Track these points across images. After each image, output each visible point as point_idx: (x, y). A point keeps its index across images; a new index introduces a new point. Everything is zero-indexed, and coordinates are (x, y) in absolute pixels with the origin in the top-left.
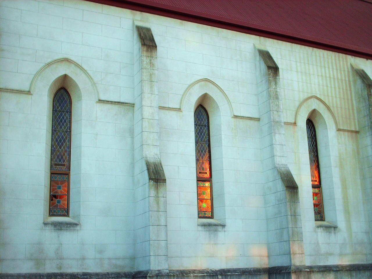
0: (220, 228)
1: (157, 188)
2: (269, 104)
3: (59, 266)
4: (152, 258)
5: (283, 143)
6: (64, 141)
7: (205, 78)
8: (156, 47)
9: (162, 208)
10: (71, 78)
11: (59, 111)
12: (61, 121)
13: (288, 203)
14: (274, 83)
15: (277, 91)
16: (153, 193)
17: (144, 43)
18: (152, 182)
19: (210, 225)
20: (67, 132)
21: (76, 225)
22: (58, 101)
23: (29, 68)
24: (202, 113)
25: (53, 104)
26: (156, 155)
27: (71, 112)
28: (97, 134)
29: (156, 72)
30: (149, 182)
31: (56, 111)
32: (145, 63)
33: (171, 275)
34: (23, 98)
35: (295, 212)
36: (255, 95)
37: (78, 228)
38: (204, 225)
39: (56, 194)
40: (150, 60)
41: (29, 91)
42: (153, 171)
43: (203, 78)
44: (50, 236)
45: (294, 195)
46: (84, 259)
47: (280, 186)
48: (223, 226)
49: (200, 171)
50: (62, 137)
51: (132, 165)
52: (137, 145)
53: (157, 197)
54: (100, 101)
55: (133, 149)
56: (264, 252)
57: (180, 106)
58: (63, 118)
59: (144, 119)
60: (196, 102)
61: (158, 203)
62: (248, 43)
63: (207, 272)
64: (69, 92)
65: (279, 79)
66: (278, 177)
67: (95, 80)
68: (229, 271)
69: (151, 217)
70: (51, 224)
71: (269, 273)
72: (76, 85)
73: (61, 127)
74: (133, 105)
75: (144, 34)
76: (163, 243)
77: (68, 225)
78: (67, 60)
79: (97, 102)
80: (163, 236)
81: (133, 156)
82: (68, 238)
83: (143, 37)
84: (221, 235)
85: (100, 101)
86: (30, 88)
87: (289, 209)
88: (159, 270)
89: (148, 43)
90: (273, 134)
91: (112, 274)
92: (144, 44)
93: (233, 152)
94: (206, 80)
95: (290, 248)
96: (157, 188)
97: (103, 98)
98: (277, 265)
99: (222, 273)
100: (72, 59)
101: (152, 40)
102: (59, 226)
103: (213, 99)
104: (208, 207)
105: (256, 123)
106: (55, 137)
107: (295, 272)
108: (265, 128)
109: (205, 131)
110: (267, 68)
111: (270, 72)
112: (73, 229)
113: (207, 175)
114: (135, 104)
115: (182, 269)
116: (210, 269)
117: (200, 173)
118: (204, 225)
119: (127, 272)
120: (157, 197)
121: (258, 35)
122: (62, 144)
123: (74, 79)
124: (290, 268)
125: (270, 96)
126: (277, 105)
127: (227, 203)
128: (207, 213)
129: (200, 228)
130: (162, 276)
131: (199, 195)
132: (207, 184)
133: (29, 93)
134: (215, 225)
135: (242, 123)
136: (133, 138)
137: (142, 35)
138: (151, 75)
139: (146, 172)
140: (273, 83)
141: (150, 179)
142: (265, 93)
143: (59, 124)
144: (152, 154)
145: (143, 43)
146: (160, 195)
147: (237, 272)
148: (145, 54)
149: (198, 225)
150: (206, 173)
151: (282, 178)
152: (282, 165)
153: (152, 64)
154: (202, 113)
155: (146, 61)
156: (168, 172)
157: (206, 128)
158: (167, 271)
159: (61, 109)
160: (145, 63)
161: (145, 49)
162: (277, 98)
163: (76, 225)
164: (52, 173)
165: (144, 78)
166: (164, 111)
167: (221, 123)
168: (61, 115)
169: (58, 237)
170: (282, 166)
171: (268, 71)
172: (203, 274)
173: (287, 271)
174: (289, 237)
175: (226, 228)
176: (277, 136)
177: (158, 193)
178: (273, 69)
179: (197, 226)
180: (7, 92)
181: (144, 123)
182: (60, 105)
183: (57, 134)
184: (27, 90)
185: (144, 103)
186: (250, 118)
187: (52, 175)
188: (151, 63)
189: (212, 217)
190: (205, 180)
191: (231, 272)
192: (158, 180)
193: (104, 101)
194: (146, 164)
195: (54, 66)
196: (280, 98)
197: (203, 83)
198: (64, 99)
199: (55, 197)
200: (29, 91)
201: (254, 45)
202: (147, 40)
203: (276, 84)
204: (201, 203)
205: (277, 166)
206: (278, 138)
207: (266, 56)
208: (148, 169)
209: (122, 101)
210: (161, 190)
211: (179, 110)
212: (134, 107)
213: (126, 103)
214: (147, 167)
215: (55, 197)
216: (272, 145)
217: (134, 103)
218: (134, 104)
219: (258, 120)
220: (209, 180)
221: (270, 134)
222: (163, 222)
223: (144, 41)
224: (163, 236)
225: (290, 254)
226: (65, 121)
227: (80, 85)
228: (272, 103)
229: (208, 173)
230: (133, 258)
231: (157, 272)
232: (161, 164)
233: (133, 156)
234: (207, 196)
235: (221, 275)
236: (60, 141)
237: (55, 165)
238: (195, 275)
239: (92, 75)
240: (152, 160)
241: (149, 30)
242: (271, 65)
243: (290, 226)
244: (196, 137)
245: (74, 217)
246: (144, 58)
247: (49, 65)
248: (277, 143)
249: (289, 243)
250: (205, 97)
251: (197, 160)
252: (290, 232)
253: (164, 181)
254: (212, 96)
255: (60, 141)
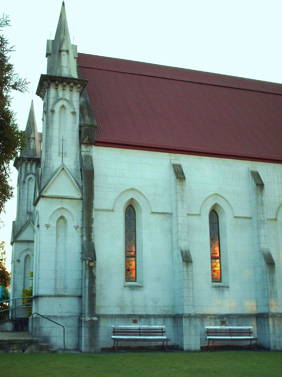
0: (225, 289)
1: (187, 266)
2: (257, 209)
3: (133, 310)
4: (185, 307)
5: (266, 235)
6: (132, 237)
7: (216, 193)
8: (185, 178)
9: (190, 278)
10: (137, 201)
11: (129, 219)
12: (130, 225)
13: (268, 274)
14: (261, 195)
15: (262, 200)
16: (185, 269)
17: (178, 176)
18: (184, 263)
19: (219, 287)
20: (133, 232)
21: (141, 287)
22: (128, 213)
23: (113, 196)
24: (214, 215)
25: (125, 215)
26: (186, 245)
27: (135, 219)
28: (151, 233)
29: (185, 194)
30: (183, 263)
31: (127, 219)
32: (178, 189)
33: (196, 317)
34: (110, 213)
35: (272, 279)
36: (249, 202)
37: (142, 289)
38: (215, 287)
39: (129, 269)
40: (182, 187)
41: (113, 210)
42: (185, 256)
43: (214, 193)
44: (127, 293)
45: (272, 268)
46: (146, 306)
47: (263, 263)
48: (228, 287)
49: (224, 199)
50: (131, 235)
51: (172, 251)
52: (175, 239)
53: (187, 271)
54: (153, 213)
55: (172, 242)
56: (254, 304)
57: (200, 213)
58: (131, 223)
59: (179, 224)
60: (210, 209)
61: (188, 275)
62: (243, 167)
63: (218, 316)
64: (134, 208)
65: (264, 192)
66: (262, 257)
67: (149, 200)
68: (231, 315)
69: (185, 283)
70: (128, 287)
71: (257, 317)
72: (139, 205)
73: (130, 229)
74: (171, 214)
75: (178, 170)
76: (191, 299)
77: (137, 287)
78: (133, 189)
79: (151, 214)
80: (191, 295)
81: (172, 245)
82: (137, 294)
83: (177, 172)
84: (226, 293)
85: (153, 213)
86: (113, 207)
87: (268, 277)
88: (189, 314)
89: (180, 176)
90: (260, 229)
91: (162, 315)
92: (178, 178)
93: (234, 240)
94: (217, 194)
95: (269, 301)
96: (187, 266)
97: (154, 211)
98: (261, 312)
99: (226, 316)
100: (135, 188)
101: (182, 173)
102: (132, 288)
103: (221, 206)
104: (218, 276)
105: (249, 220)
106: (127, 235)
107: (272, 317)
108: (255, 224)
109: (216, 227)
110: (256, 185)
111: (258, 188)
112: (140, 289)
113: (218, 255)
114: (173, 214)
115: (202, 313)
116: (220, 313)
117: (213, 254)
118: (215, 287)
119: (171, 315)
120: (187, 271)
121: (251, 160)
122: (131, 239)
123: (137, 200)
124: (269, 314)
125: (258, 204)
126: (262, 209)
127: (230, 272)
128: (217, 279)
129: (213, 289)
130: (191, 317)
131: (212, 267)
132: (218, 261)
133: (113, 210)
134: (223, 287)
135: (240, 221)
136: (172, 234)
137: (176, 171)
138: (182, 197)
139: (181, 257)
140: (260, 195)
141: (183, 261)
142: (255, 201)
143: (129, 227)
144: (183, 245)
145: (177, 177)
146: (189, 270)
147: (236, 316)
148: (178, 183)
149: (212, 287)
150: (217, 254)
151: (264, 258)
152: (265, 249)
153: (183, 190)
154: (214, 215)
155: (179, 188)
156: (193, 255)
157: (217, 225)
158: (194, 314)
159: (130, 218)
160: (178, 189)
161: (178, 180)
162: (263, 205)
163: (141, 287)
164: (126, 257)
165: (179, 199)
166: (190, 216)
167: (226, 221)
168: (130, 221)
169: (132, 294)
170: (265, 249)
171: (257, 187)
172: (215, 316)
173: (267, 316)
174: (268, 294)
175: (230, 289)
176: (262, 230)
177: (188, 269)
178: (260, 185)
179: (253, 217)
180: (101, 211)
181: (179, 227)
182: (129, 215)
183: (128, 233)
184: (112, 209)
185: (179, 215)
186: (246, 218)
187: (127, 258)
188: (182, 189)
189: (220, 281)
190: (216, 258)
191: (232, 316)
192: (188, 261)
193: (154, 213)
194: (181, 251)
195: (125, 193)
196: (265, 204)
197: (214, 196)
198: (131, 211)
199: (128, 270)
200: (113, 210)
201: (248, 167)
202: (179, 174)
203: (262, 195)
204: (214, 273)
205: (262, 249)
206: (263, 231)
207: (256, 176)
208: (182, 255)
209: (165, 212)
210: (190, 267)
211: (200, 215)
212: (172, 215)
213: (167, 213)
214: (182, 254)
215: (128, 270)
216: (259, 236)
217: (172, 212)
218: (172, 213)
219: (251, 218)
220: (219, 258)
221: (258, 229)
222: (191, 286)
223: (177, 175)
224: (191, 295)
225: (268, 305)
226: (132, 225)
227: (141, 204)
228: (259, 208)
229: (218, 254)
230: (173, 307)
231: (188, 315)
232: (189, 251)
233: (172, 245)
234: (218, 269)
235: (226, 317)
236: (130, 237)
237: (128, 251)
238: (211, 317)
239: (147, 197)
240: (184, 249)
241: (180, 166)
242: (258, 182)
243: (269, 288)
244: (210, 231)
245: (139, 282)
246: (178, 187)
247: (123, 193)
248: (263, 235)
249: (268, 299)
250: (216, 205)
251: (211, 246)
252: (269, 292)
253: (192, 262)
254: (220, 205)
255: (130, 237)
